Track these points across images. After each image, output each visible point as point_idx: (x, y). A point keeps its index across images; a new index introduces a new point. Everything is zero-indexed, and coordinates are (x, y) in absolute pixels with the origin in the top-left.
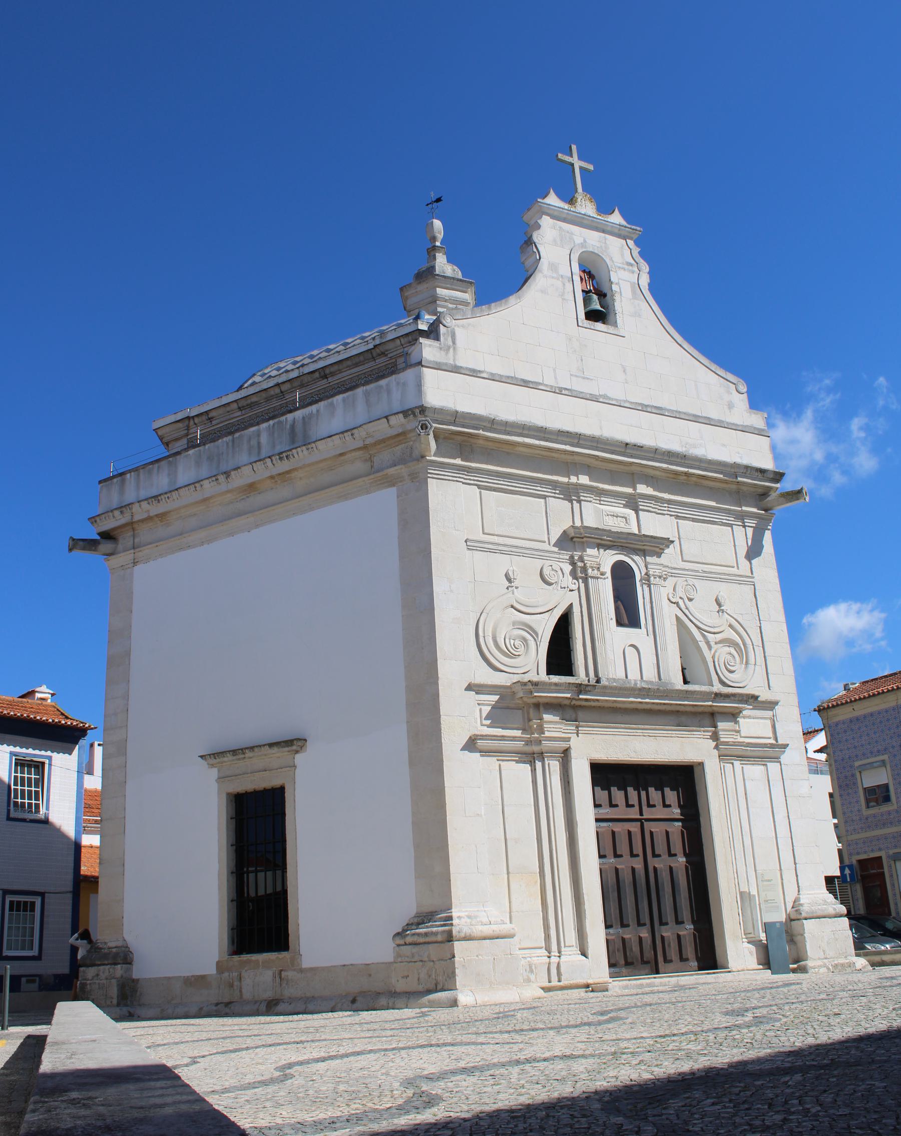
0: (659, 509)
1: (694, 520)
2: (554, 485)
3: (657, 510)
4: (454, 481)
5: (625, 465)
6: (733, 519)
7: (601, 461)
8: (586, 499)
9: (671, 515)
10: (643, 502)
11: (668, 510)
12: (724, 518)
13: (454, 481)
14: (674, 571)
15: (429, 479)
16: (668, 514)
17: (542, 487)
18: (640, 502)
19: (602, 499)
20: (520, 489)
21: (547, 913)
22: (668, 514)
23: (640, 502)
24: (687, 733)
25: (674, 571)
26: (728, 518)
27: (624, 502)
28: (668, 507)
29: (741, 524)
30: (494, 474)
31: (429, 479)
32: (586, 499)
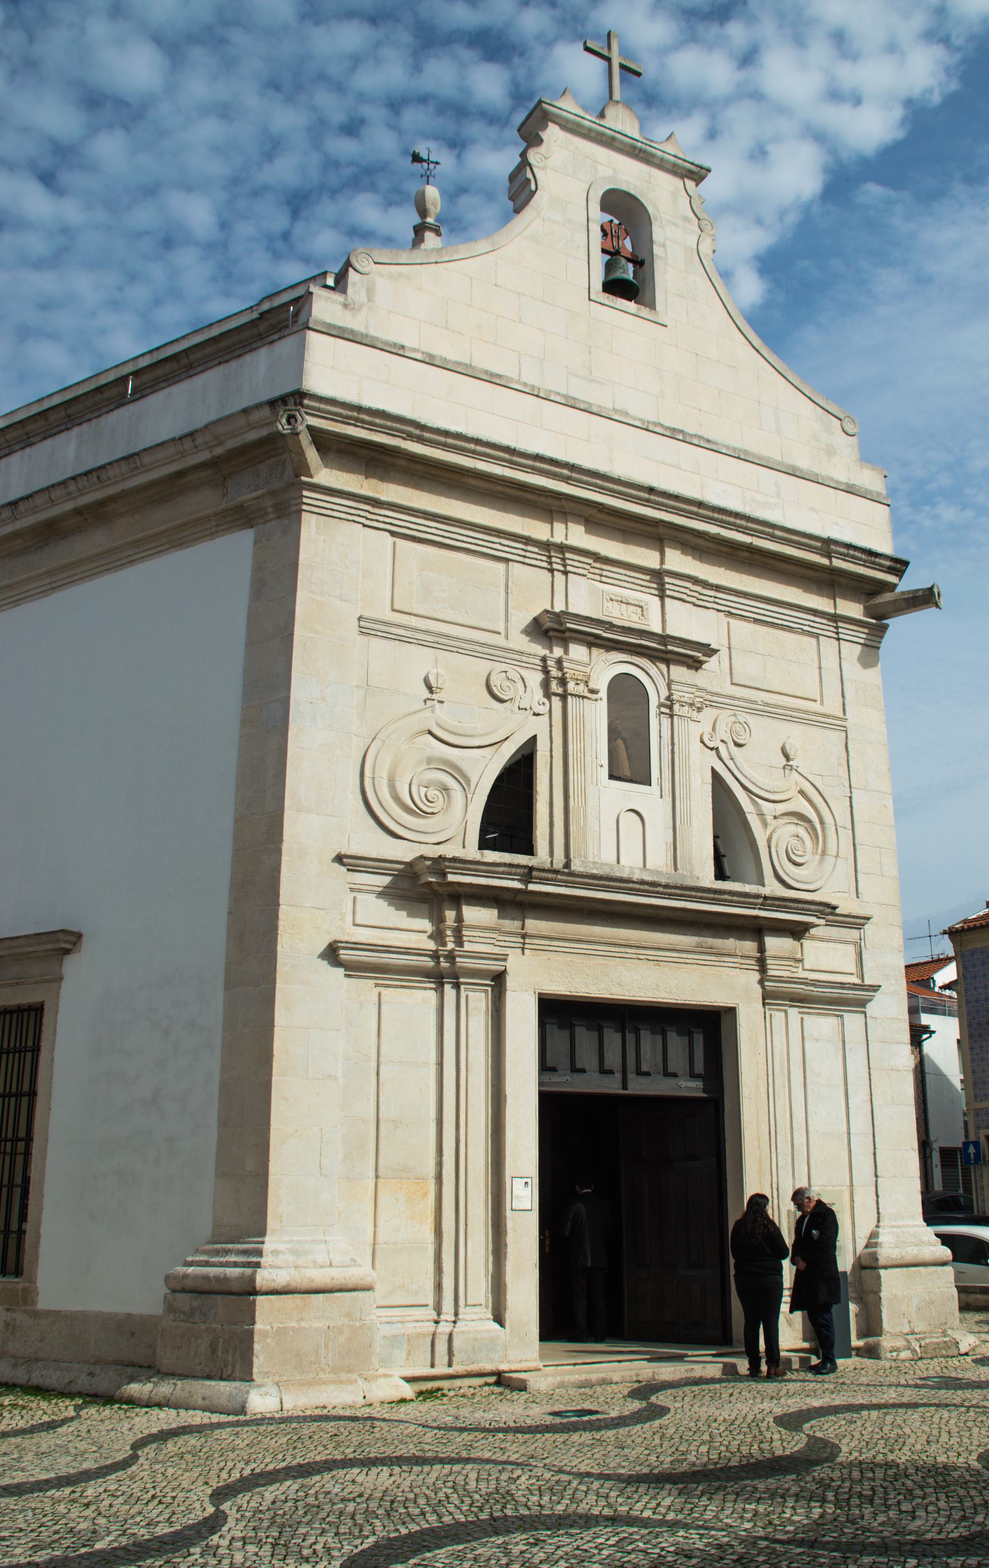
11: (715, 602)
24: (713, 958)
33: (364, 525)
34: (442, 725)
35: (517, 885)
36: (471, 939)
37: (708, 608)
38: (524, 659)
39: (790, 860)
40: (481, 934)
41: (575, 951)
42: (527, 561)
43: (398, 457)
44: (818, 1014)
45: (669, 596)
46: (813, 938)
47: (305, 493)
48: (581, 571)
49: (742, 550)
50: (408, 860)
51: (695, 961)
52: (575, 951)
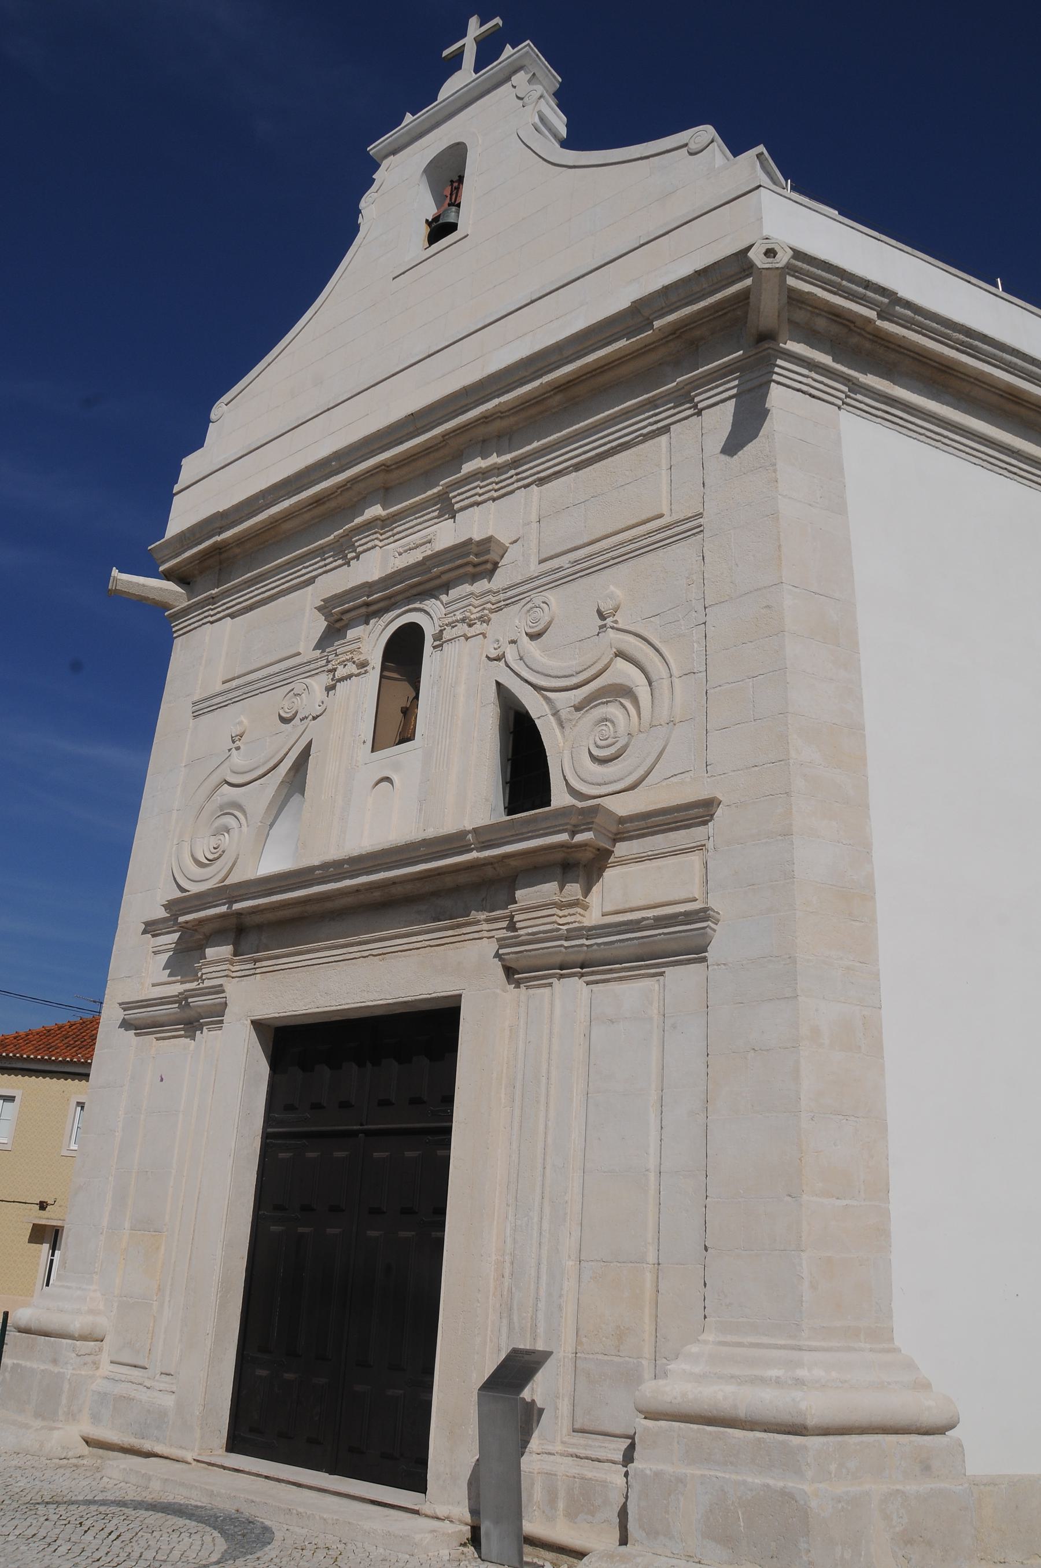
0: (212, 616)
1: (577, 467)
2: (320, 552)
3: (212, 613)
4: (200, 626)
5: (437, 450)
6: (331, 559)
7: (397, 468)
8: (365, 547)
9: (526, 486)
10: (459, 494)
11: (518, 481)
12: (644, 423)
13: (200, 626)
14: (510, 594)
15: (773, 384)
16: (519, 488)
17: (307, 567)
18: (455, 497)
19: (395, 531)
20: (609, 446)
21: (229, 1470)
22: (519, 488)
23: (455, 497)
24: (450, 933)
25: (510, 594)
26: (654, 419)
27: (736, 382)
28: (517, 474)
29: (691, 411)
30: (702, 380)
31: (773, 384)
32: (365, 547)
33: (212, 623)
34: (236, 771)
35: (223, 909)
36: (209, 976)
37: (512, 492)
38: (312, 666)
39: (603, 761)
40: (214, 969)
41: (300, 964)
42: (328, 567)
43: (280, 524)
44: (621, 979)
45: (774, 381)
46: (622, 862)
47: (779, 362)
48: (370, 545)
49: (550, 397)
50: (607, 869)
51: (428, 943)
52: (300, 964)
